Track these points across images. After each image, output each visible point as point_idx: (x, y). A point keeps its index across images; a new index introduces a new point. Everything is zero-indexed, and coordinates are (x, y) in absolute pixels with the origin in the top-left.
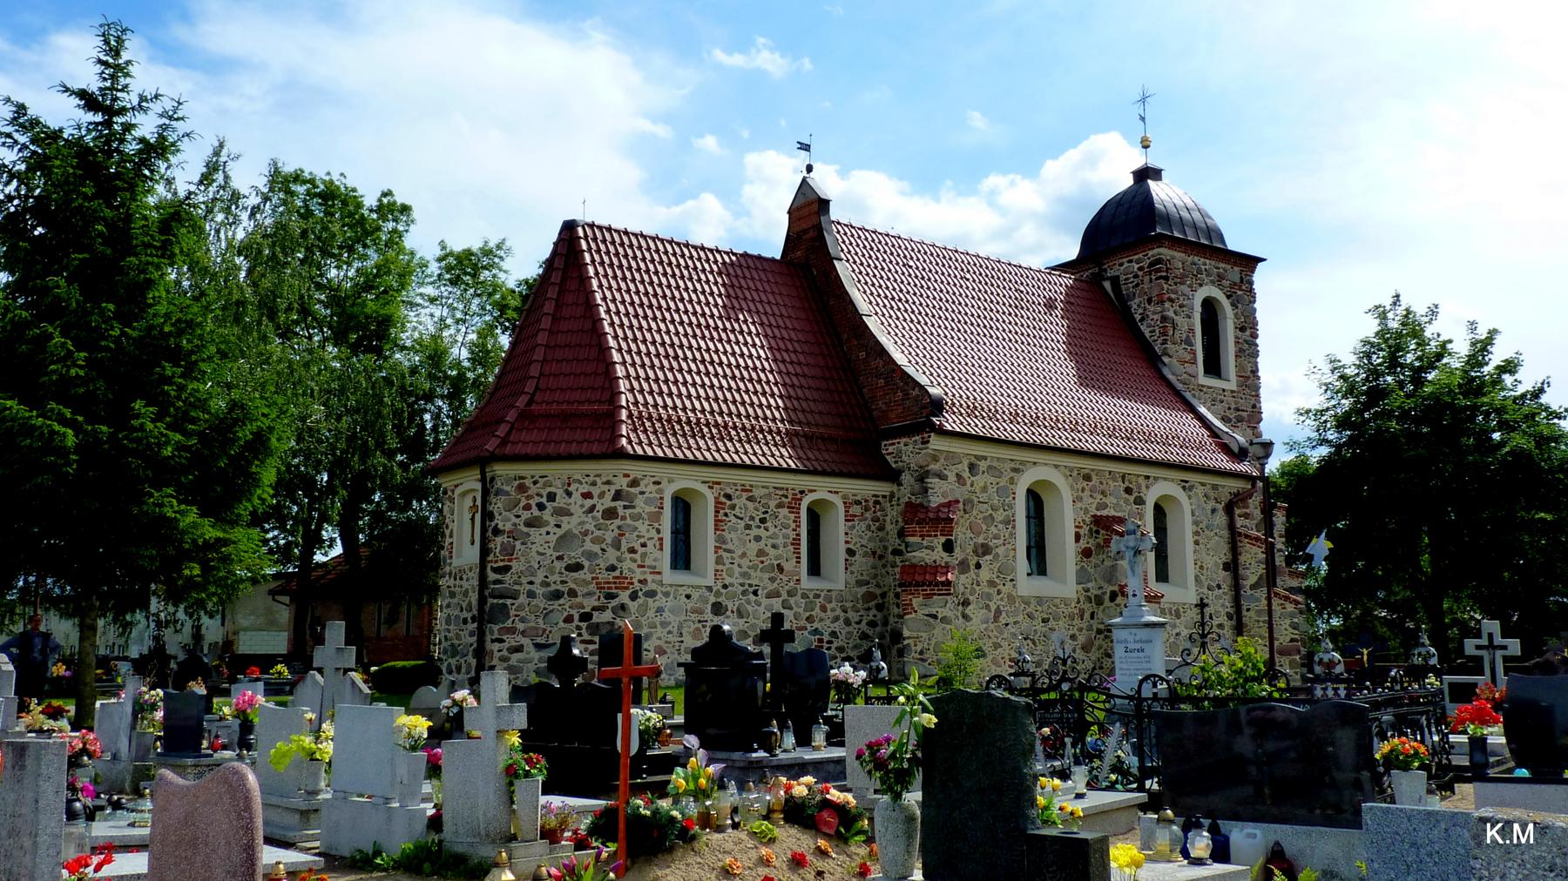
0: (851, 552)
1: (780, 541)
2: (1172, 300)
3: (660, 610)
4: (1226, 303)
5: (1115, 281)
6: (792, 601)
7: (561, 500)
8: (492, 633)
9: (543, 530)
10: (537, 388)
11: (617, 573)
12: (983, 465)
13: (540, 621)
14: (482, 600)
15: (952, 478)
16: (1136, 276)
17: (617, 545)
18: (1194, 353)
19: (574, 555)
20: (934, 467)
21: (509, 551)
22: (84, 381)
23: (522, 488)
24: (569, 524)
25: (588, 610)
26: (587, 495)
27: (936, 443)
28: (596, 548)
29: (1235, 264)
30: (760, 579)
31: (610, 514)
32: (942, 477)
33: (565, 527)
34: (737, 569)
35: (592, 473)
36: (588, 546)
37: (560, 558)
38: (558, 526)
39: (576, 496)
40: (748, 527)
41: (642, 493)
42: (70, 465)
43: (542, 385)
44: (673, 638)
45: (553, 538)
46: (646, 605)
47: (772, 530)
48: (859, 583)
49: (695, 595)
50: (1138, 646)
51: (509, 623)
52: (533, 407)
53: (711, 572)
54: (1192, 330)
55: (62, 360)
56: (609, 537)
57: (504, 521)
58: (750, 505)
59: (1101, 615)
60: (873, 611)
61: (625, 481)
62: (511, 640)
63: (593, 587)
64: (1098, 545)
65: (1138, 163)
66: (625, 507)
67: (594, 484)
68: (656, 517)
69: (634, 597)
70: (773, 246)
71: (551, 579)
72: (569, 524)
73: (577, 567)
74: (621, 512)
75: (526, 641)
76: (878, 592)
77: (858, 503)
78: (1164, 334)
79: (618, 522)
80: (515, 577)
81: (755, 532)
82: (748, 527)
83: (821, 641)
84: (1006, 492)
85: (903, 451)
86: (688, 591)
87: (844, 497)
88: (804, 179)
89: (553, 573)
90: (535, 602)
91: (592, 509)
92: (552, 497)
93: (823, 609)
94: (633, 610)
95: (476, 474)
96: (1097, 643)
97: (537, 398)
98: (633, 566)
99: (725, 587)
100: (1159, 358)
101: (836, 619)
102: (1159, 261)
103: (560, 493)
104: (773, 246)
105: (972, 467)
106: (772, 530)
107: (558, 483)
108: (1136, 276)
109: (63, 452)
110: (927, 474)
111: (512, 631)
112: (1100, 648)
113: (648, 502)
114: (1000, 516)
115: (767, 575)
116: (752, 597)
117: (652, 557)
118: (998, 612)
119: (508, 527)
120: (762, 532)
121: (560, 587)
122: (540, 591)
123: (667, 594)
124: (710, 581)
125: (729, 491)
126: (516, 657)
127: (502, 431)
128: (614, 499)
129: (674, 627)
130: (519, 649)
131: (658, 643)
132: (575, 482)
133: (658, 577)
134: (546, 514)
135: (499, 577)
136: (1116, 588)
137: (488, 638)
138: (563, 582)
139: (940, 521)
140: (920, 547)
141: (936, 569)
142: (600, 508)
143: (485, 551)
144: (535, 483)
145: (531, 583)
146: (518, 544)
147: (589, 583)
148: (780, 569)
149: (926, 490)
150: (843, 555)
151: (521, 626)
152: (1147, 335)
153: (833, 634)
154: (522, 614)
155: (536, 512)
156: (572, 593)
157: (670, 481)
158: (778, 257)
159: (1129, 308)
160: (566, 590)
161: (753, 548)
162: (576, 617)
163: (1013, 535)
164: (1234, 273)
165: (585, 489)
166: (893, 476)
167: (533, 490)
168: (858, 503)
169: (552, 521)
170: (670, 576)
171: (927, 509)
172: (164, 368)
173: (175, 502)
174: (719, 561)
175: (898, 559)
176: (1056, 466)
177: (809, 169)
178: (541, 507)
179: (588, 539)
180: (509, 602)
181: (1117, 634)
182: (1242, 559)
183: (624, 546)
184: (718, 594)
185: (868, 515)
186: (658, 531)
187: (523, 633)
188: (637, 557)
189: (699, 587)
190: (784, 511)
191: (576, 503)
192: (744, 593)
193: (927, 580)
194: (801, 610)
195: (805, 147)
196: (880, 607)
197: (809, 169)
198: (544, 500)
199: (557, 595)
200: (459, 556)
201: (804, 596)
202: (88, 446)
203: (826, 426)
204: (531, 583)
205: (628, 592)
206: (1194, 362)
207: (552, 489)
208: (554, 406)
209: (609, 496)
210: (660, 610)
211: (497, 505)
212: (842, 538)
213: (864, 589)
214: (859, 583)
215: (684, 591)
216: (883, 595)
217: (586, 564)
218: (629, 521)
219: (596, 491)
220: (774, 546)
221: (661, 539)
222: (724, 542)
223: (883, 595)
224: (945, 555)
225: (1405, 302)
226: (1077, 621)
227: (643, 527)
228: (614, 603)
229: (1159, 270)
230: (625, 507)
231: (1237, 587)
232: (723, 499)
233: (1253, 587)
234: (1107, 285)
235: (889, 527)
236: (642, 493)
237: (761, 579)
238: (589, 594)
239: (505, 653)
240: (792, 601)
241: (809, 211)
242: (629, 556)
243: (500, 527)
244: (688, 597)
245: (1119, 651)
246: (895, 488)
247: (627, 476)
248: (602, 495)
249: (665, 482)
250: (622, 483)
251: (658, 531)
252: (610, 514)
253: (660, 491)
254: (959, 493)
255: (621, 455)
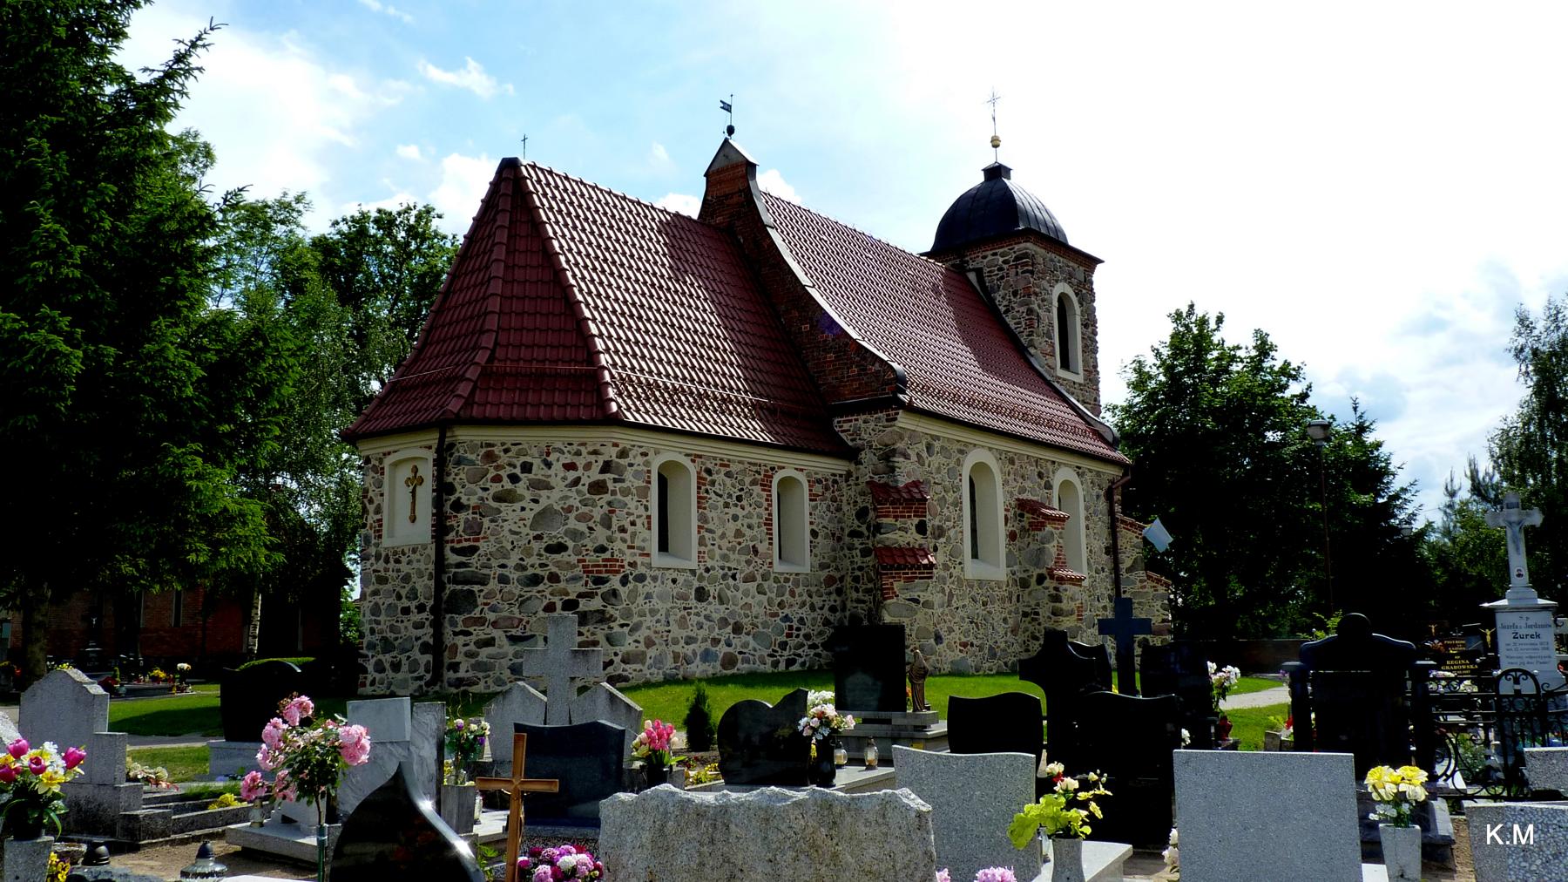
0: (814, 534)
1: (754, 521)
2: (1036, 294)
3: (648, 596)
4: (1075, 299)
5: (979, 272)
6: (766, 585)
7: (538, 471)
8: (453, 623)
9: (517, 506)
10: (496, 343)
11: (607, 555)
12: (937, 444)
13: (515, 610)
14: (440, 587)
15: (914, 458)
16: (1001, 269)
17: (606, 522)
18: (1052, 345)
19: (556, 533)
20: (900, 445)
21: (475, 529)
22: (81, 285)
23: (490, 457)
24: (548, 499)
25: (573, 596)
26: (570, 467)
27: (904, 421)
28: (582, 527)
29: (1081, 264)
30: (738, 561)
31: (598, 488)
32: (907, 457)
33: (544, 503)
34: (718, 552)
35: (576, 442)
36: (573, 523)
37: (538, 538)
38: (536, 501)
39: (557, 467)
40: (727, 505)
41: (631, 465)
42: (64, 399)
43: (503, 339)
44: (660, 628)
45: (529, 515)
46: (635, 590)
47: (748, 509)
48: (823, 566)
49: (681, 580)
50: (1532, 631)
51: (476, 613)
52: (496, 364)
53: (695, 555)
54: (1051, 324)
55: (48, 255)
56: (597, 514)
57: (468, 494)
58: (728, 481)
59: (1026, 598)
60: (834, 596)
61: (614, 451)
62: (479, 633)
63: (578, 571)
64: (1023, 529)
65: (989, 162)
66: (615, 480)
67: (578, 453)
68: (643, 492)
69: (624, 581)
70: (690, 206)
71: (528, 562)
72: (548, 499)
73: (560, 548)
74: (610, 485)
75: (498, 634)
76: (837, 575)
77: (819, 481)
78: (1031, 326)
79: (607, 497)
80: (484, 560)
81: (732, 511)
82: (727, 505)
83: (791, 628)
84: (954, 473)
85: (864, 429)
86: (674, 576)
87: (808, 475)
88: (726, 141)
89: (530, 555)
90: (508, 588)
91: (576, 482)
92: (527, 468)
93: (792, 594)
94: (624, 596)
95: (433, 438)
96: (1023, 626)
97: (500, 353)
98: (624, 547)
99: (707, 570)
100: (1026, 349)
101: (804, 604)
102: (1026, 255)
103: (537, 463)
104: (690, 206)
105: (929, 447)
106: (748, 509)
107: (535, 451)
108: (1001, 269)
109: (57, 381)
110: (894, 452)
111: (481, 621)
112: (1026, 630)
113: (637, 475)
114: (950, 497)
115: (744, 558)
116: (731, 581)
117: (641, 537)
118: (951, 595)
119: (474, 501)
120: (738, 511)
121: (539, 571)
122: (514, 575)
123: (655, 579)
124: (694, 565)
125: (710, 466)
126: (485, 652)
127: (464, 389)
128: (603, 471)
129: (661, 616)
130: (490, 642)
131: (647, 633)
132: (557, 454)
133: (646, 560)
134: (521, 488)
135: (463, 559)
136: (1044, 571)
137: (448, 630)
138: (542, 565)
139: (913, 500)
140: (893, 528)
141: (916, 552)
142: (586, 481)
143: (441, 529)
144: (506, 451)
145: (503, 566)
146: (486, 521)
147: (574, 566)
148: (756, 551)
149: (893, 469)
150: (808, 536)
151: (491, 616)
152: (1013, 327)
153: (801, 620)
154: (493, 602)
155: (507, 484)
156: (554, 578)
157: (657, 452)
158: (695, 216)
159: (993, 300)
160: (544, 573)
161: (732, 527)
162: (559, 605)
163: (960, 517)
164: (1080, 273)
165: (567, 459)
166: (850, 454)
167: (504, 459)
168: (819, 481)
169: (528, 495)
170: (657, 559)
171: (898, 490)
172: (176, 277)
173: (199, 460)
174: (702, 542)
175: (857, 542)
176: (990, 449)
177: (731, 130)
178: (514, 479)
179: (572, 516)
180: (476, 588)
181: (1501, 619)
182: (1120, 543)
183: (615, 525)
184: (701, 578)
185: (828, 494)
186: (646, 508)
187: (495, 624)
188: (627, 536)
189: (684, 570)
190: (757, 489)
191: (557, 475)
192: (724, 577)
193: (909, 563)
194: (773, 595)
195: (727, 108)
196: (839, 592)
197: (731, 130)
198: (518, 471)
199: (535, 580)
200: (391, 535)
201: (776, 580)
202: (94, 370)
203: (782, 399)
204: (503, 566)
205: (619, 577)
206: (1053, 356)
207: (528, 459)
208: (534, 365)
209: (596, 468)
210: (648, 596)
211: (458, 476)
212: (807, 519)
213: (825, 573)
214: (823, 566)
215: (671, 575)
216: (842, 579)
217: (570, 544)
218: (619, 496)
219: (580, 462)
220: (750, 527)
221: (649, 517)
222: (706, 522)
223: (842, 579)
224: (918, 537)
225: (1199, 312)
226: (1007, 605)
227: (632, 503)
228: (605, 588)
229: (1026, 264)
230: (615, 480)
231: (1116, 569)
232: (704, 475)
233: (1129, 570)
234: (972, 276)
235: (845, 508)
236: (631, 465)
237: (739, 562)
238: (575, 579)
239: (472, 647)
240: (766, 585)
241: (730, 177)
242: (618, 535)
243: (464, 500)
244: (674, 581)
245: (1505, 638)
246: (852, 467)
247: (616, 445)
248: (588, 466)
249: (651, 453)
250: (611, 453)
251: (646, 508)
252: (598, 488)
253: (647, 464)
254: (919, 475)
255: (617, 421)
